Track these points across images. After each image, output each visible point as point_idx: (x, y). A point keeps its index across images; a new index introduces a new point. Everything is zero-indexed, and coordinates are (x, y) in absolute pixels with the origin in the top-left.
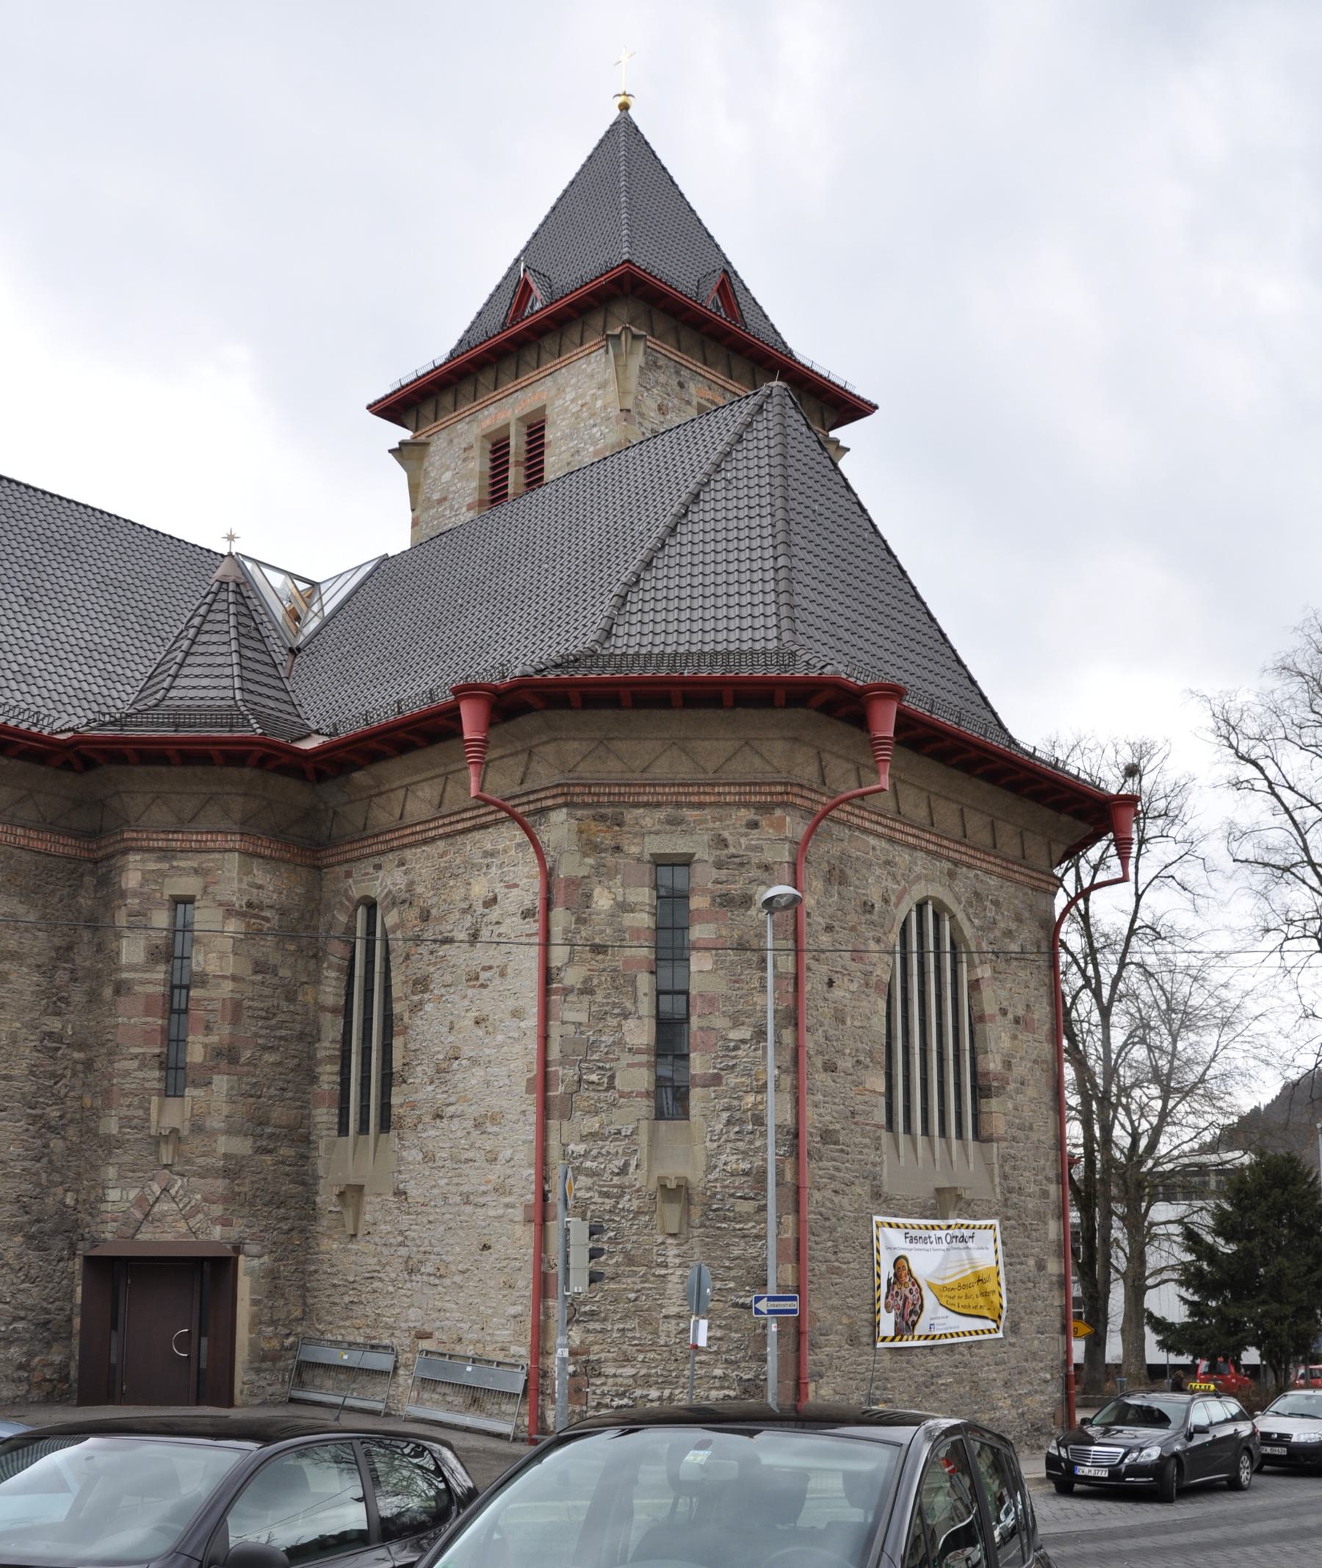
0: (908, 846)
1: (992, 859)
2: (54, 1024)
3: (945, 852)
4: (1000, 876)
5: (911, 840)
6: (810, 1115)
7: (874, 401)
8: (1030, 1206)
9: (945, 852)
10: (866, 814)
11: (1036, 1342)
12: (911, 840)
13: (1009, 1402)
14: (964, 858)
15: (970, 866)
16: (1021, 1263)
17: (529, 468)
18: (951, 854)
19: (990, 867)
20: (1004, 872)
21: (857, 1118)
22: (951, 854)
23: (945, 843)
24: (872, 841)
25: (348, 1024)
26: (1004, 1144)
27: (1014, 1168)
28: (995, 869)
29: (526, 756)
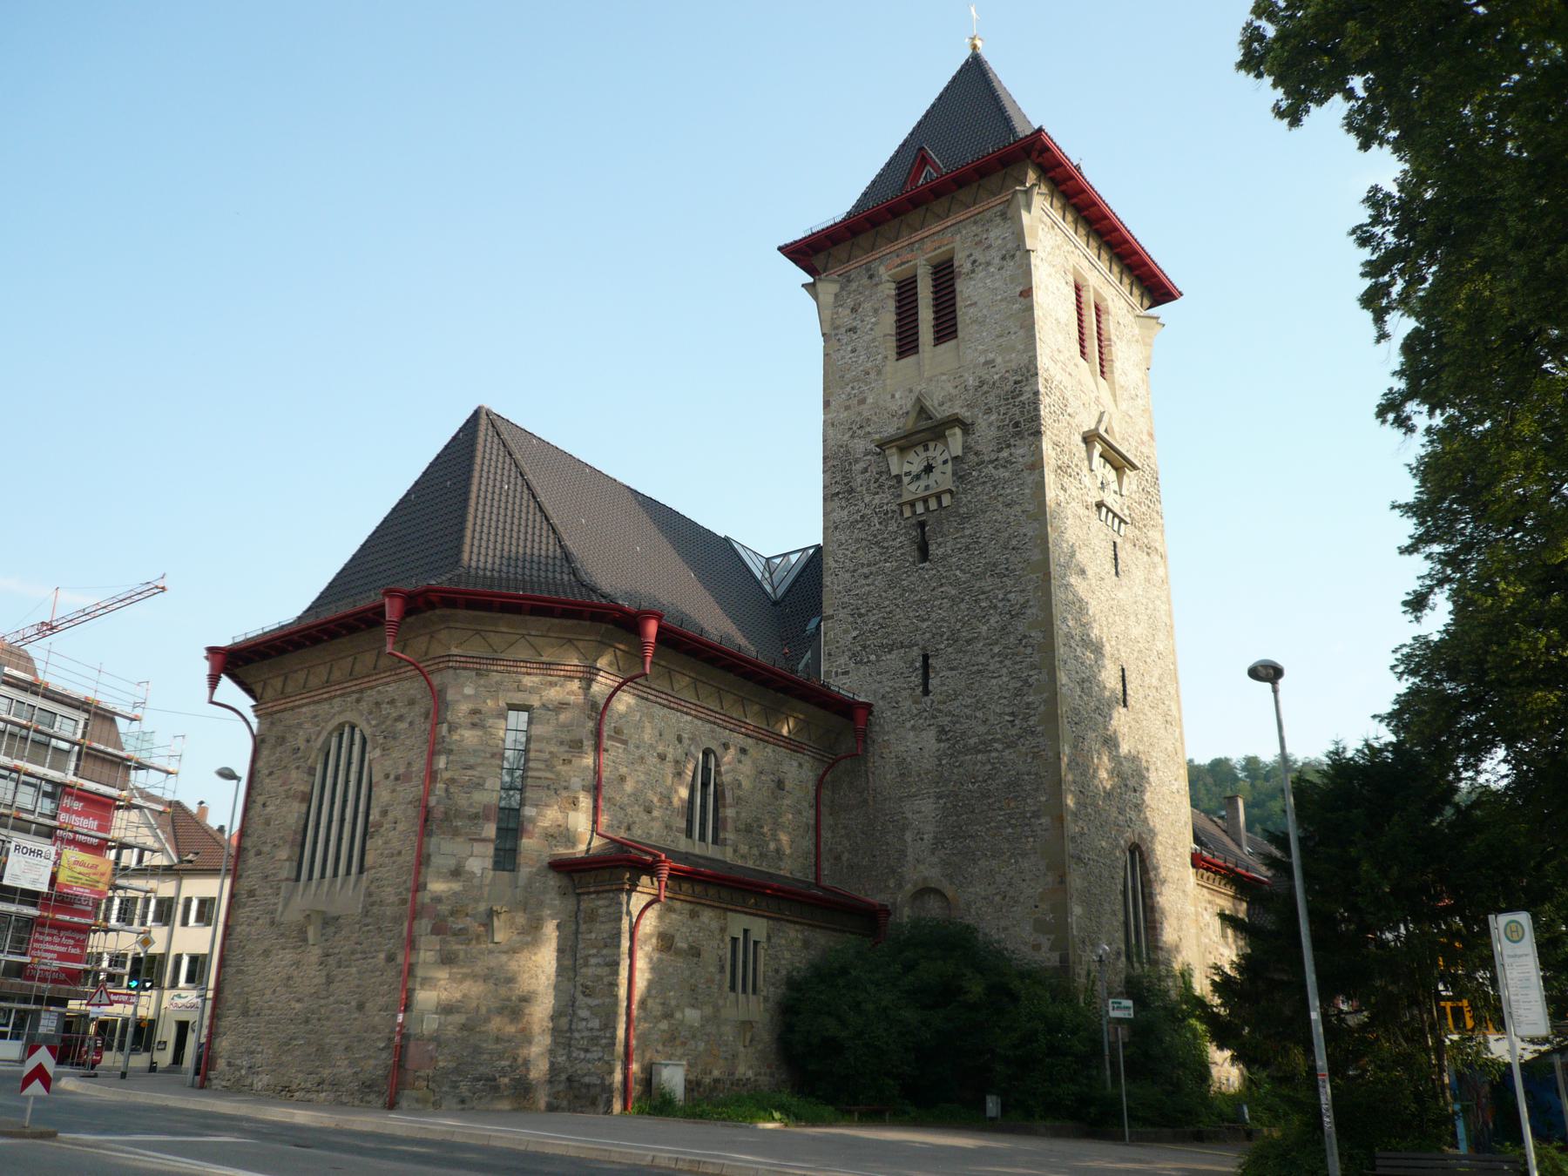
0: (326, 700)
1: (383, 675)
2: (13, 918)
3: (349, 690)
4: (395, 681)
5: (325, 696)
6: (589, 760)
7: (779, 253)
8: (388, 913)
9: (349, 690)
10: (293, 699)
11: (377, 1018)
12: (325, 696)
13: (346, 1062)
14: (363, 686)
15: (372, 688)
16: (373, 958)
17: (899, 301)
18: (354, 688)
19: (385, 680)
20: (395, 677)
21: (269, 879)
22: (354, 688)
23: (346, 685)
24: (304, 710)
25: (309, 807)
26: (373, 871)
27: (378, 887)
28: (388, 679)
29: (428, 636)
